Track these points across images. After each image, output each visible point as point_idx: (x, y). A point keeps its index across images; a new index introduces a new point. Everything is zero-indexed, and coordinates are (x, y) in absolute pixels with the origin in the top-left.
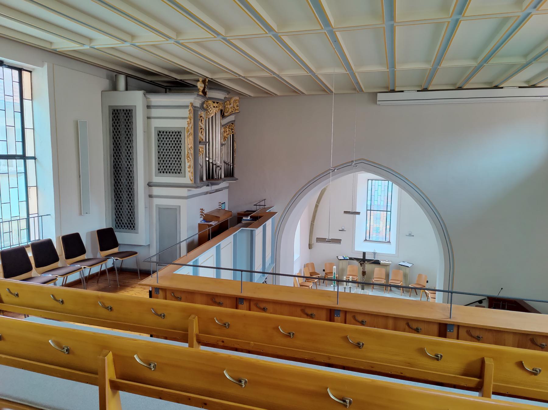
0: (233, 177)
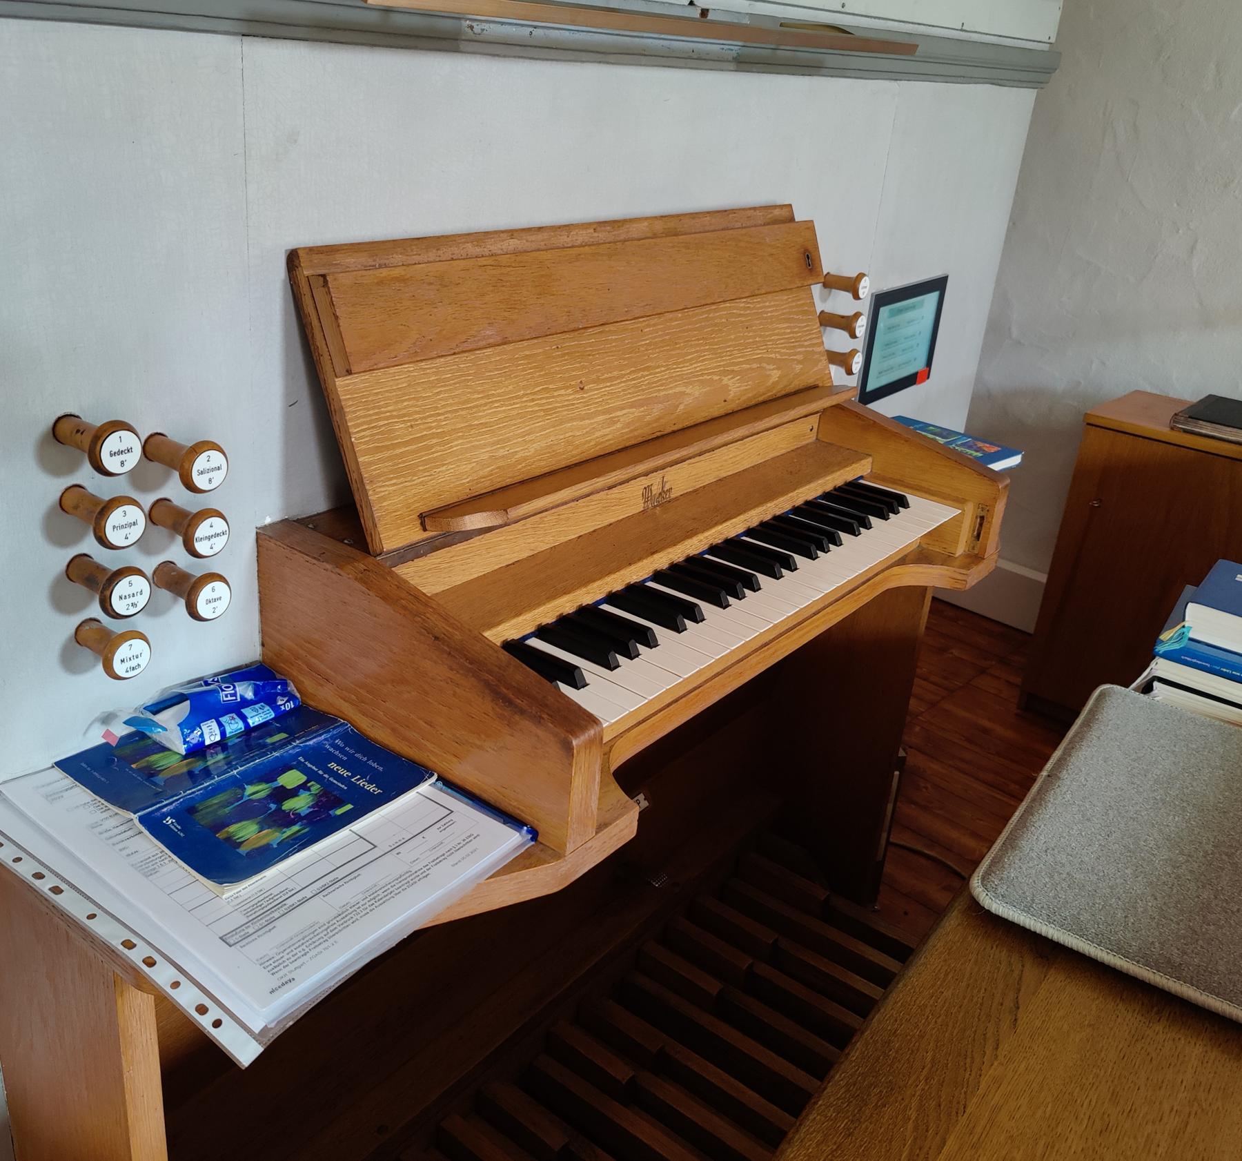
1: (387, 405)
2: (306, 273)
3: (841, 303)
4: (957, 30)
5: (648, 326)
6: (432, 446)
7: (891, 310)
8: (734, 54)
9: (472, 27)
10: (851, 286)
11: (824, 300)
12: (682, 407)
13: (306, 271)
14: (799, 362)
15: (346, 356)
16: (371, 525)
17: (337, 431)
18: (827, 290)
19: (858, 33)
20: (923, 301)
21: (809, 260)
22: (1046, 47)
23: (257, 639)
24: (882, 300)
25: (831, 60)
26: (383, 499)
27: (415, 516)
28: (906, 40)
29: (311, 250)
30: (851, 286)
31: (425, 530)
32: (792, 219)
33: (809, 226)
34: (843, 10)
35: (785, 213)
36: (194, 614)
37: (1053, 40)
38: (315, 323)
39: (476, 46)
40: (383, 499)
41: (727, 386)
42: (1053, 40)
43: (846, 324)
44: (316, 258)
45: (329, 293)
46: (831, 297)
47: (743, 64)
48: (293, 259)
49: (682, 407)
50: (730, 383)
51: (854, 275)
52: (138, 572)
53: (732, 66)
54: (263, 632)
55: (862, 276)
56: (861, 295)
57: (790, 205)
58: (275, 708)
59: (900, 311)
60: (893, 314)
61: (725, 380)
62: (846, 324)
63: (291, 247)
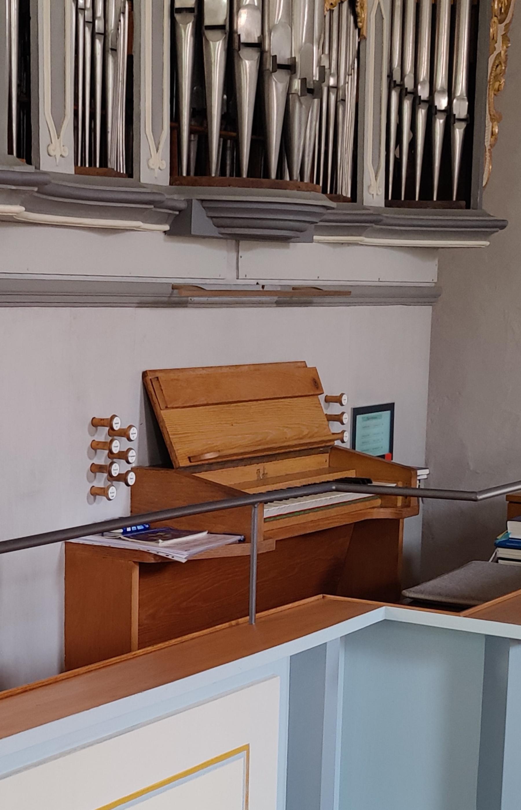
0: (468, 207)
1: (175, 421)
2: (150, 378)
3: (334, 409)
4: (376, 281)
5: (253, 405)
6: (188, 436)
7: (363, 418)
8: (275, 300)
9: (191, 299)
10: (338, 400)
11: (327, 408)
12: (269, 437)
13: (149, 377)
14: (317, 427)
15: (165, 402)
16: (175, 458)
17: (161, 428)
18: (327, 404)
19: (325, 289)
20: (381, 416)
21: (316, 384)
22: (433, 285)
23: (129, 509)
24: (357, 412)
25: (316, 299)
26: (178, 450)
27: (187, 457)
28: (346, 289)
29: (150, 371)
30: (338, 400)
31: (191, 462)
32: (306, 367)
33: (315, 369)
34: (318, 279)
35: (303, 364)
36: (109, 499)
37: (436, 281)
38: (153, 393)
39: (192, 305)
40: (178, 450)
41: (286, 432)
42: (436, 281)
43: (338, 418)
44: (151, 373)
45: (159, 382)
46: (330, 407)
47: (279, 304)
48: (145, 374)
49: (269, 437)
50: (287, 431)
51: (339, 395)
52: (132, 449)
53: (275, 305)
54: (132, 507)
55: (342, 394)
56: (344, 404)
57: (291, 656)
58: (144, 526)
59: (368, 419)
60: (365, 420)
61: (285, 430)
62: (338, 418)
63: (145, 370)
